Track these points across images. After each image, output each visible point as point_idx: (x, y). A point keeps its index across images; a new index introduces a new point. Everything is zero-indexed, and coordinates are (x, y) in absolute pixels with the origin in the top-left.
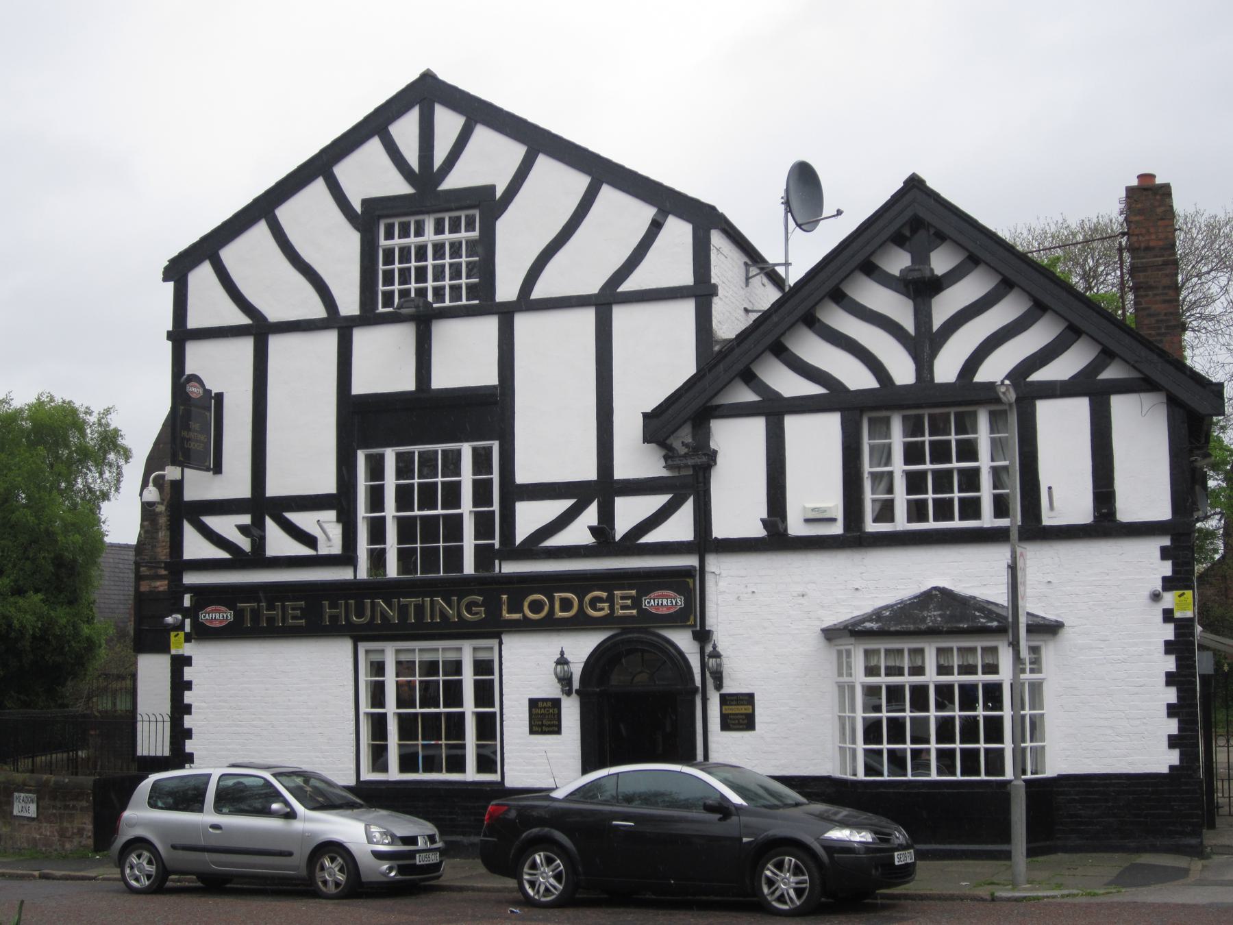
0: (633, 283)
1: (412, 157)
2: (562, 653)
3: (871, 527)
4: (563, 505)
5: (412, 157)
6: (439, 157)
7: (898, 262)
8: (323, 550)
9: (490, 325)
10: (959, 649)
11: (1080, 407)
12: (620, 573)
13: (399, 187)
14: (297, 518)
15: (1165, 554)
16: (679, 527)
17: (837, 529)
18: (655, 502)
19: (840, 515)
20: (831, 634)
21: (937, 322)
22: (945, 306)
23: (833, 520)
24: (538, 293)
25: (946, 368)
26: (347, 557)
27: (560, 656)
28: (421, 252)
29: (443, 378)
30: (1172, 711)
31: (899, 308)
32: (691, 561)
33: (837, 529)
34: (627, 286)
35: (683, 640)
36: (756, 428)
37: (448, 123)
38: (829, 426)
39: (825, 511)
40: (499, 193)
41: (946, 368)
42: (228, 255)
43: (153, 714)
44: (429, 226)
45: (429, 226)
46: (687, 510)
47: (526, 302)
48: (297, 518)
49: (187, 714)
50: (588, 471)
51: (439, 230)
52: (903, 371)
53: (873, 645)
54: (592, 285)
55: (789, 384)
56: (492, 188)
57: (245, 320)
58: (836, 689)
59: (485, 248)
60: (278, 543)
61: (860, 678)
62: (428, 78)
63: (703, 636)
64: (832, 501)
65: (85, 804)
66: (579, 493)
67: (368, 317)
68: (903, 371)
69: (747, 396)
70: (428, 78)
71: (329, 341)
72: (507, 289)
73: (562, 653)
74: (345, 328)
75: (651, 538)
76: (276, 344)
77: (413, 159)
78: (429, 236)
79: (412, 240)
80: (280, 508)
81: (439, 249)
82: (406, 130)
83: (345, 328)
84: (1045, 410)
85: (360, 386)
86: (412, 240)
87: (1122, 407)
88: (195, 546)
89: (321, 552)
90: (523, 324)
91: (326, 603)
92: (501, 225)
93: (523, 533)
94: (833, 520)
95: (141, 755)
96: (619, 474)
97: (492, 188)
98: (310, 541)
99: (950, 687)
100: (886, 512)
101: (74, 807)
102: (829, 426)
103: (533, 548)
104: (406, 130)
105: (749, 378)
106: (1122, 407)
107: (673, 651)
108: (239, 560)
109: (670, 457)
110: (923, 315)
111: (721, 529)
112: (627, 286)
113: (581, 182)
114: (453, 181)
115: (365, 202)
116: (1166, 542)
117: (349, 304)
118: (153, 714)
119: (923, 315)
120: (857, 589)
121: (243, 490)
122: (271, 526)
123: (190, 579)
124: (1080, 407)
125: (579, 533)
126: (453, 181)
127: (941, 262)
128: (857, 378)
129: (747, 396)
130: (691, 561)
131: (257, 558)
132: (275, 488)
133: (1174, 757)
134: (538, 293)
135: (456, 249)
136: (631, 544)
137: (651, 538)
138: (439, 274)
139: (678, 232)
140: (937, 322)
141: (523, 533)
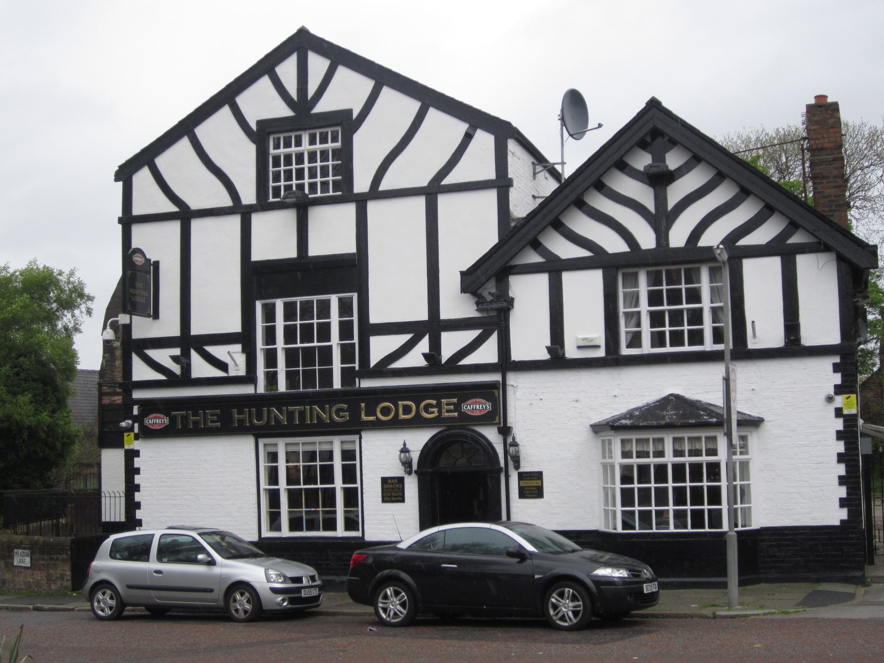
2: (405, 444)
3: (625, 351)
6: (312, 89)
7: (642, 161)
8: (232, 373)
9: (349, 211)
11: (774, 264)
14: (214, 350)
15: (836, 368)
16: (488, 353)
17: (601, 353)
18: (471, 335)
19: (602, 343)
20: (597, 429)
21: (671, 203)
22: (676, 192)
23: (598, 347)
24: (384, 186)
25: (678, 237)
26: (250, 378)
28: (300, 158)
30: (842, 480)
31: (644, 195)
32: (496, 377)
33: (601, 353)
34: (447, 181)
35: (491, 434)
36: (542, 281)
37: (317, 65)
38: (595, 279)
39: (592, 340)
41: (678, 237)
42: (161, 162)
44: (305, 139)
45: (305, 139)
46: (493, 341)
47: (375, 193)
48: (214, 350)
50: (422, 314)
51: (312, 142)
52: (647, 239)
54: (423, 181)
55: (565, 250)
56: (350, 112)
59: (345, 155)
60: (200, 368)
61: (618, 460)
63: (505, 431)
64: (597, 333)
65: (65, 556)
66: (416, 330)
67: (263, 205)
68: (647, 239)
69: (535, 258)
71: (234, 223)
72: (361, 184)
73: (405, 444)
74: (245, 213)
76: (197, 225)
78: (306, 147)
79: (293, 149)
80: (201, 343)
81: (312, 157)
82: (287, 70)
83: (245, 213)
84: (749, 266)
85: (257, 255)
86: (293, 149)
87: (805, 264)
88: (141, 371)
90: (374, 208)
92: (357, 138)
93: (375, 357)
94: (598, 347)
95: (104, 521)
97: (350, 112)
98: (223, 366)
100: (635, 340)
101: (57, 559)
102: (595, 279)
103: (383, 369)
104: (287, 70)
105: (536, 245)
106: (805, 264)
108: (172, 381)
109: (480, 303)
110: (660, 199)
111: (517, 354)
112: (447, 181)
114: (321, 107)
115: (260, 123)
116: (837, 359)
117: (249, 196)
119: (660, 199)
120: (615, 396)
124: (774, 264)
125: (415, 358)
126: (321, 107)
127: (673, 161)
128: (614, 244)
129: (535, 258)
130: (496, 377)
131: (186, 379)
132: (197, 329)
133: (843, 514)
134: (384, 186)
135: (324, 155)
136: (453, 366)
137: (467, 361)
138: (313, 175)
139: (484, 141)
140: (671, 203)
141: (375, 357)
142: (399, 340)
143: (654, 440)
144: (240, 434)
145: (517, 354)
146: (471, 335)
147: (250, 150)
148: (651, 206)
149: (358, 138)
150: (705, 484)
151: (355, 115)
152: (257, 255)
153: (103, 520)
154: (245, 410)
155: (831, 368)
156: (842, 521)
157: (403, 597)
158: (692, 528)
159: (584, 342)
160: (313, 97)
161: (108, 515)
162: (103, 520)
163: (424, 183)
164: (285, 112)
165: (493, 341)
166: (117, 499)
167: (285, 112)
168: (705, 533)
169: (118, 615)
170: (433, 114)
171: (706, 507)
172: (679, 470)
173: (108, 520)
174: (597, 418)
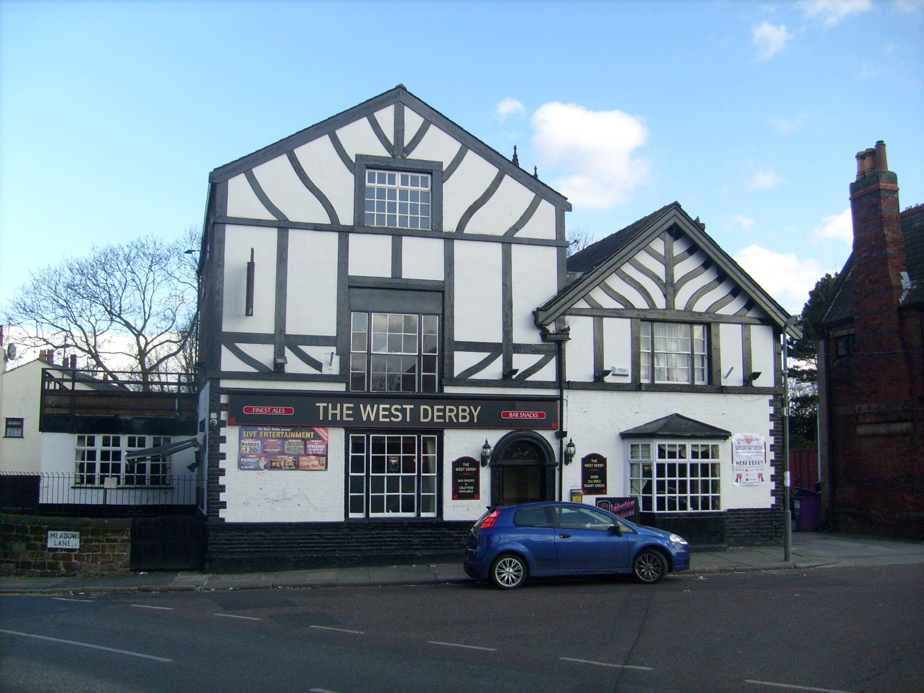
0: (519, 234)
1: (390, 134)
2: (486, 442)
4: (484, 355)
5: (390, 134)
8: (326, 371)
10: (642, 445)
12: (291, 393)
13: (379, 151)
14: (308, 350)
15: (771, 403)
16: (548, 373)
17: (628, 380)
18: (537, 358)
19: (629, 373)
20: (625, 436)
21: (677, 277)
22: (680, 270)
23: (627, 375)
25: (680, 302)
27: (485, 443)
29: (409, 272)
31: (659, 270)
33: (628, 380)
35: (548, 435)
37: (413, 121)
38: (624, 326)
39: (625, 371)
40: (445, 168)
41: (680, 302)
43: (52, 473)
47: (460, 234)
48: (308, 350)
49: (221, 475)
50: (497, 337)
53: (635, 442)
54: (500, 230)
57: (270, 217)
58: (629, 466)
60: (294, 365)
62: (401, 88)
63: (561, 434)
64: (626, 365)
65: (125, 537)
66: (493, 349)
67: (361, 226)
68: (660, 302)
70: (401, 88)
71: (334, 237)
72: (450, 224)
73: (486, 442)
74: (344, 232)
75: (477, 376)
76: (293, 234)
77: (391, 138)
80: (295, 343)
83: (344, 232)
88: (229, 362)
89: (323, 373)
90: (458, 245)
91: (412, 406)
92: (446, 186)
93: (458, 370)
94: (627, 375)
95: (109, 504)
96: (271, 330)
98: (317, 365)
99: (108, 452)
101: (115, 540)
102: (624, 326)
103: (463, 379)
104: (386, 117)
107: (546, 443)
108: (264, 373)
109: (545, 335)
110: (669, 274)
111: (570, 376)
112: (519, 234)
113: (283, 160)
114: (414, 155)
115: (358, 157)
116: (771, 397)
117: (346, 218)
118: (52, 473)
119: (669, 274)
120: (637, 413)
121: (269, 328)
122: (288, 353)
123: (225, 384)
125: (495, 370)
128: (639, 302)
131: (278, 371)
132: (292, 328)
134: (468, 230)
135: (414, 194)
136: (522, 381)
137: (477, 376)
138: (403, 208)
140: (677, 277)
141: (458, 370)
142: (478, 357)
143: (642, 445)
144: (460, 429)
145: (570, 376)
146: (537, 358)
147: (349, 179)
148: (662, 276)
149: (448, 187)
150: (677, 478)
151: (445, 168)
152: (353, 271)
153: (40, 502)
154: (317, 404)
155: (768, 403)
156: (772, 505)
157: (520, 567)
158: (702, 509)
159: (620, 371)
160: (409, 145)
161: (45, 496)
162: (40, 502)
163: (501, 233)
164: (383, 152)
165: (552, 365)
166: (66, 480)
167: (383, 152)
168: (676, 514)
169: (529, 582)
170: (300, 152)
171: (677, 495)
172: (660, 467)
173: (45, 502)
174: (623, 429)
